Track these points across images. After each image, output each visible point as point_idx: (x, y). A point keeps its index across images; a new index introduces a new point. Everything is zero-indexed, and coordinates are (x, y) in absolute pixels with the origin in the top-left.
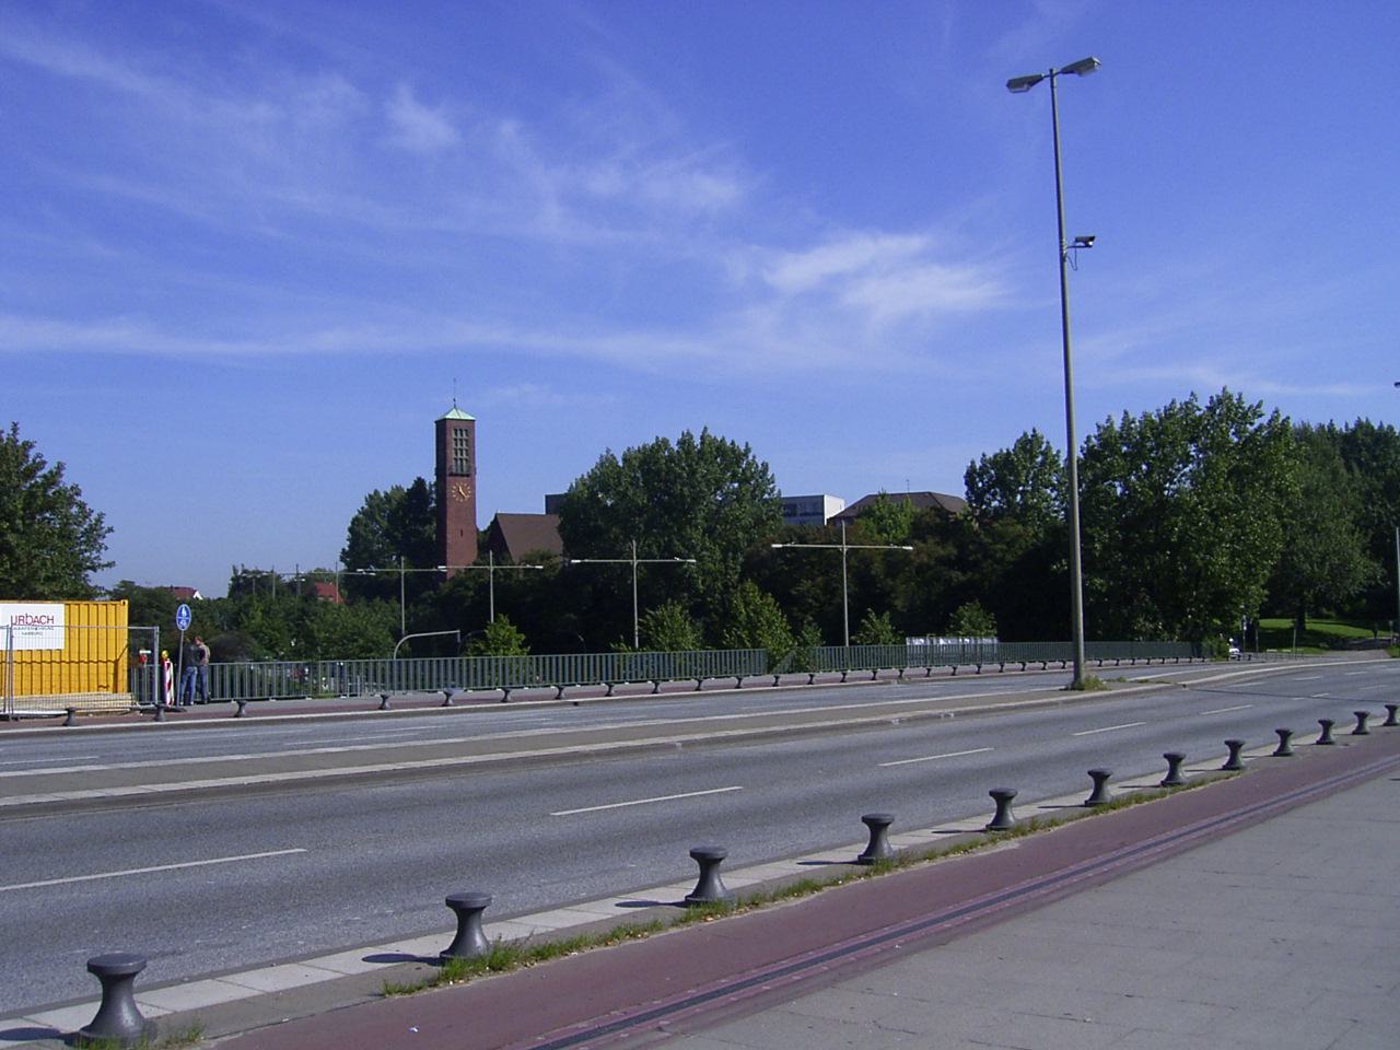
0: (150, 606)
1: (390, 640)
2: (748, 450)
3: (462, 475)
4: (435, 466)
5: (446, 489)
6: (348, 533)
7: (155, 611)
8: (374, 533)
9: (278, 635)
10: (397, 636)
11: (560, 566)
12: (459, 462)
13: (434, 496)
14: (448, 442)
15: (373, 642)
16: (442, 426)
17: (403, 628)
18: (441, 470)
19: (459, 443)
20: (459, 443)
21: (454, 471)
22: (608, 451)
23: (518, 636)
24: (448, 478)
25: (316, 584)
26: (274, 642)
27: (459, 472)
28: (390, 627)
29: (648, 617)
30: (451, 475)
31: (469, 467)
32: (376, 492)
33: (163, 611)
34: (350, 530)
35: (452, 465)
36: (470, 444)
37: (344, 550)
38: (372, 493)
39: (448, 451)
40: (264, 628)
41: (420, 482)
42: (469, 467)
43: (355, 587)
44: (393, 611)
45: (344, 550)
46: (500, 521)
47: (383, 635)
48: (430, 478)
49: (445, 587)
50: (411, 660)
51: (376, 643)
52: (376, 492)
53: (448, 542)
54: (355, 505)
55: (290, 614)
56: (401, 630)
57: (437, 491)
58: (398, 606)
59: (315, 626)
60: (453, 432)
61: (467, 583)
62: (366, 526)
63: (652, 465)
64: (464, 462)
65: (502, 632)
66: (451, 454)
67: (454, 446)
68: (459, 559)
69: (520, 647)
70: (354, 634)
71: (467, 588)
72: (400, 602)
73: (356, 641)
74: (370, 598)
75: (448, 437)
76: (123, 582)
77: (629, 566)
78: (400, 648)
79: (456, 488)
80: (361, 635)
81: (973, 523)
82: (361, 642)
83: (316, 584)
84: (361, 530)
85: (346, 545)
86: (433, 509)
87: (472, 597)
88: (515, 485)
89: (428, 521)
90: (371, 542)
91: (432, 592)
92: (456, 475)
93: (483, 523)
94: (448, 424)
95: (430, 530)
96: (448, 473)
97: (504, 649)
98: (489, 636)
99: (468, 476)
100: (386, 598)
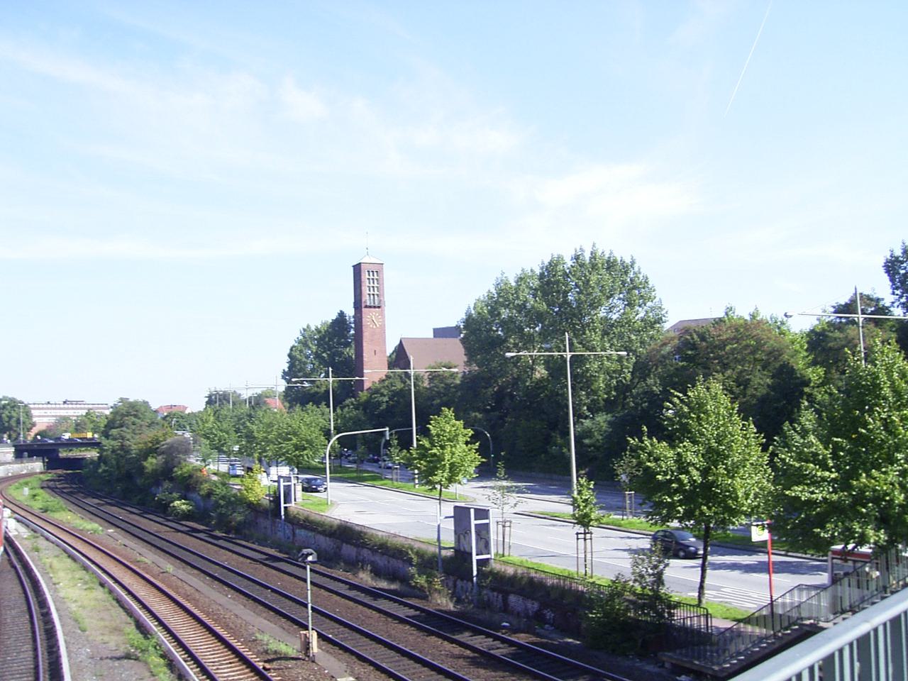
0: (128, 414)
1: (322, 438)
2: (633, 263)
3: (375, 307)
4: (353, 301)
5: (361, 319)
6: (288, 358)
7: (133, 419)
8: (307, 357)
9: (226, 436)
10: (328, 435)
11: (460, 375)
12: (372, 296)
13: (353, 325)
14: (363, 280)
15: (307, 441)
16: (357, 269)
17: (332, 429)
18: (358, 305)
19: (371, 281)
20: (371, 273)
21: (368, 304)
22: (503, 273)
23: (465, 432)
24: (364, 310)
25: (266, 399)
26: (223, 442)
27: (372, 304)
28: (321, 428)
29: (676, 400)
30: (366, 307)
31: (380, 301)
32: (308, 326)
33: (139, 418)
34: (290, 356)
35: (366, 299)
36: (381, 282)
37: (284, 370)
38: (305, 327)
39: (363, 288)
40: (214, 431)
41: (342, 314)
42: (380, 301)
43: (296, 398)
44: (323, 414)
45: (284, 370)
46: (404, 343)
47: (316, 435)
48: (350, 312)
49: (363, 396)
50: (473, 522)
51: (310, 442)
52: (308, 326)
53: (365, 359)
54: (291, 337)
55: (241, 419)
56: (330, 430)
57: (355, 322)
58: (327, 410)
59: (255, 427)
60: (367, 273)
61: (382, 390)
62: (301, 351)
63: (550, 281)
64: (376, 296)
65: (448, 428)
66: (365, 291)
67: (368, 284)
68: (374, 372)
69: (467, 443)
70: (287, 434)
71: (382, 395)
72: (329, 407)
73: (291, 440)
74: (303, 404)
75: (363, 277)
76: (121, 399)
77: (563, 359)
78: (331, 446)
79: (369, 316)
80: (295, 434)
81: (270, 453)
82: (295, 440)
83: (266, 399)
84: (297, 354)
85: (286, 367)
86: (353, 335)
87: (387, 402)
88: (420, 315)
89: (347, 345)
90: (305, 363)
91: (353, 399)
92: (370, 307)
93: (390, 348)
94: (363, 266)
95: (350, 352)
96: (363, 305)
97: (451, 447)
98: (433, 432)
99: (379, 307)
100: (317, 403)
